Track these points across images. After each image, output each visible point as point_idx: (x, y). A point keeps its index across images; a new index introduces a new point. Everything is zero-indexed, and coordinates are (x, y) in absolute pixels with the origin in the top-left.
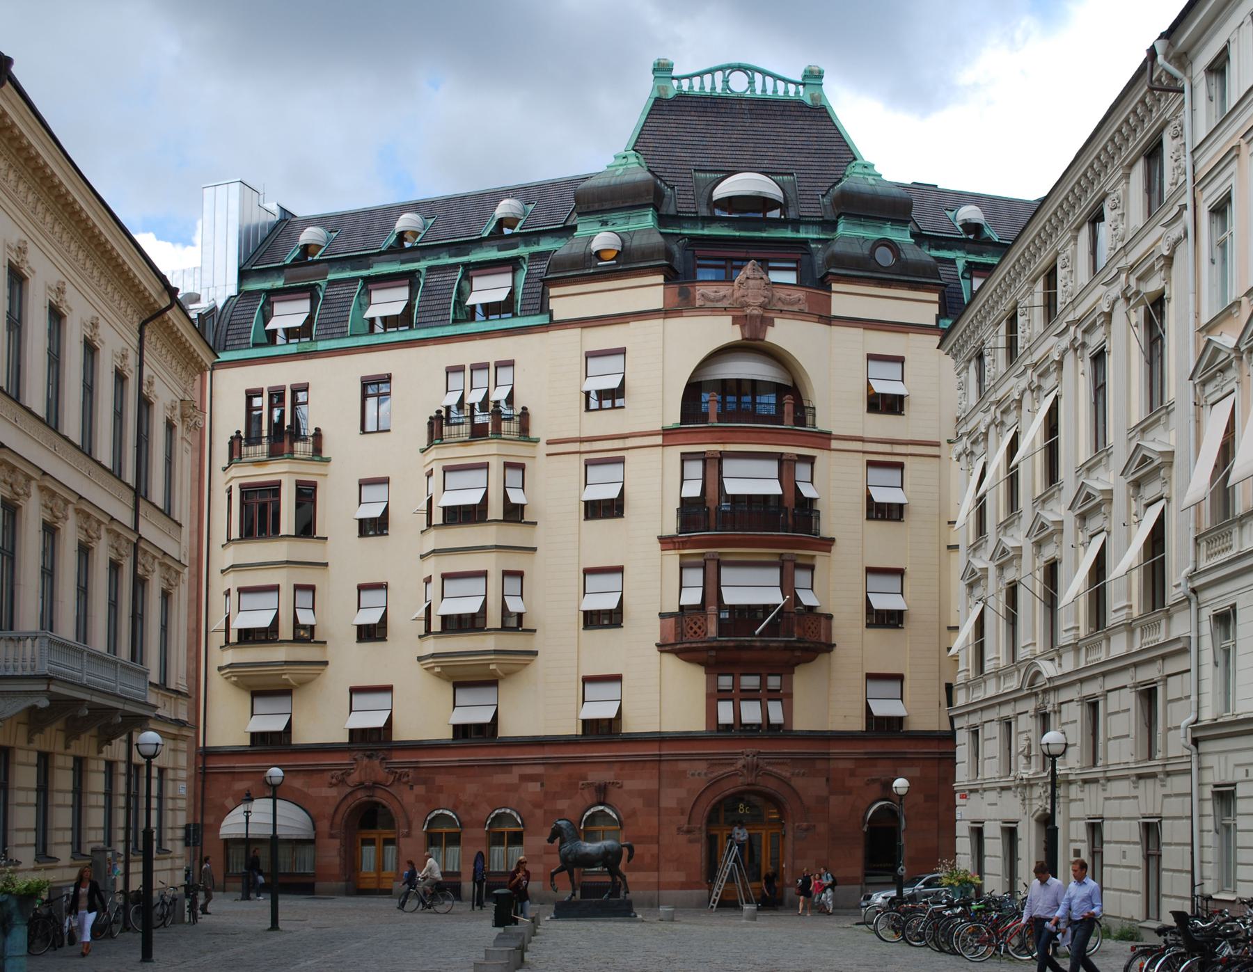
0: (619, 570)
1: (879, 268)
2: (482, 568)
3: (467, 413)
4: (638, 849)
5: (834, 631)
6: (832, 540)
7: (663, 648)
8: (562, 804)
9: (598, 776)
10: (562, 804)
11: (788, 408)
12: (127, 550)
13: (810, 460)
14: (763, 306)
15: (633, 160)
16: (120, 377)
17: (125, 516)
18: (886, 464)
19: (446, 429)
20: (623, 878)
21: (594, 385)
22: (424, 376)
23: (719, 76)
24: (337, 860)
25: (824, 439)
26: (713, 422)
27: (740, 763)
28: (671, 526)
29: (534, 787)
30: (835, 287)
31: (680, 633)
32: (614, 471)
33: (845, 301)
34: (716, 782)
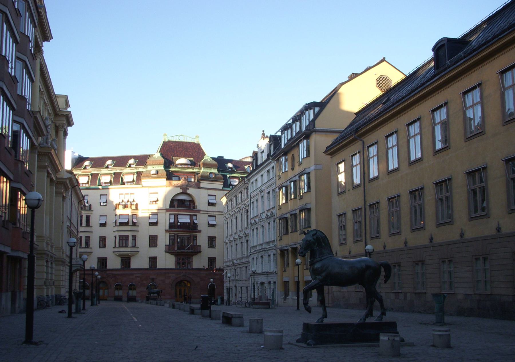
6: (201, 231)
7: (166, 251)
9: (151, 277)
11: (191, 205)
13: (196, 215)
18: (212, 216)
25: (199, 211)
28: (168, 228)
29: (138, 279)
31: (169, 249)
33: (203, 184)
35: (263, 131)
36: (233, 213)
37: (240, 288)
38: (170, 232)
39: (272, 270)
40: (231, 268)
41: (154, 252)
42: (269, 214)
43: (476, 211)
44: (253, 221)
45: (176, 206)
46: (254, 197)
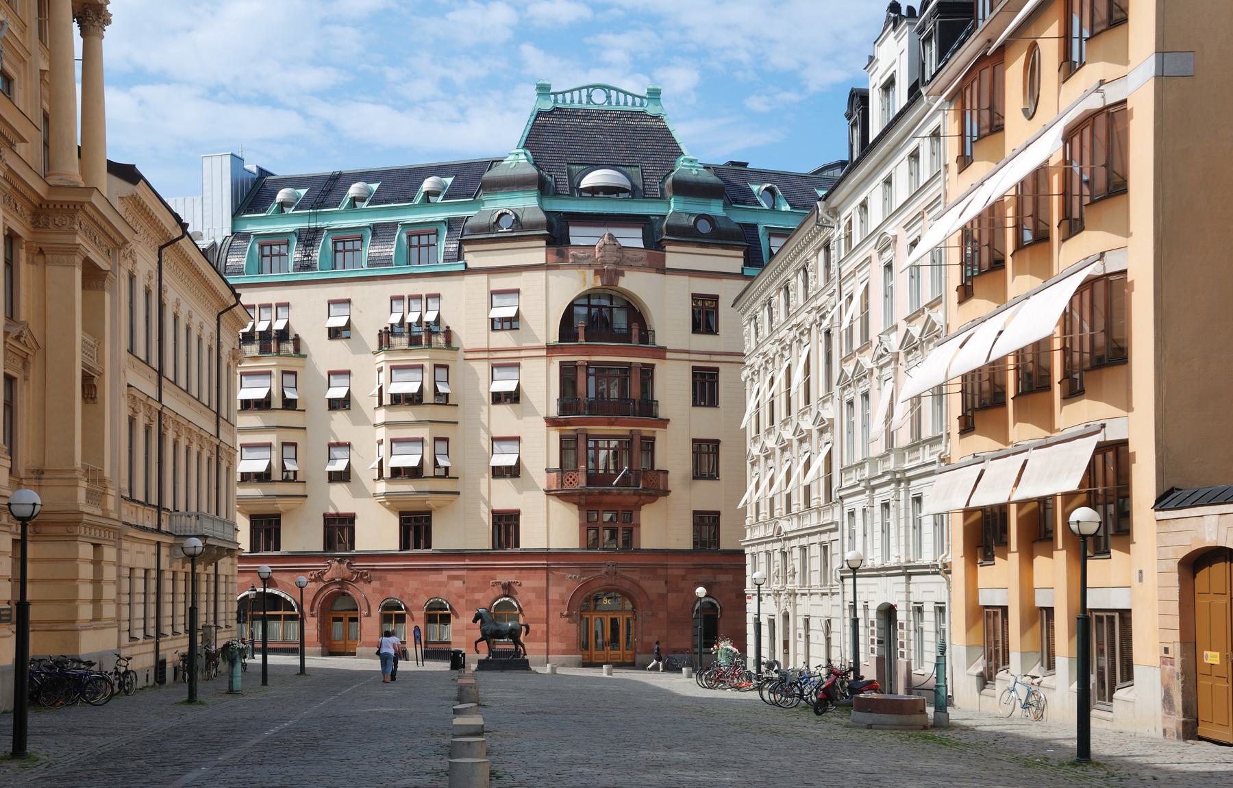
0: (518, 439)
2: (420, 436)
3: (406, 330)
4: (532, 627)
5: (669, 482)
6: (668, 420)
8: (478, 596)
9: (505, 578)
10: (478, 596)
11: (635, 332)
12: (156, 417)
14: (616, 263)
15: (522, 156)
16: (148, 293)
17: (152, 391)
19: (392, 339)
20: (523, 646)
21: (498, 313)
22: (373, 306)
23: (584, 92)
24: (316, 632)
25: (661, 352)
26: (582, 340)
27: (603, 571)
30: (668, 248)
32: (513, 373)
33: (675, 257)
34: (587, 583)
36: (777, 347)
37: (800, 623)
39: (927, 558)
40: (769, 547)
41: (504, 496)
42: (916, 329)
44: (849, 368)
45: (581, 333)
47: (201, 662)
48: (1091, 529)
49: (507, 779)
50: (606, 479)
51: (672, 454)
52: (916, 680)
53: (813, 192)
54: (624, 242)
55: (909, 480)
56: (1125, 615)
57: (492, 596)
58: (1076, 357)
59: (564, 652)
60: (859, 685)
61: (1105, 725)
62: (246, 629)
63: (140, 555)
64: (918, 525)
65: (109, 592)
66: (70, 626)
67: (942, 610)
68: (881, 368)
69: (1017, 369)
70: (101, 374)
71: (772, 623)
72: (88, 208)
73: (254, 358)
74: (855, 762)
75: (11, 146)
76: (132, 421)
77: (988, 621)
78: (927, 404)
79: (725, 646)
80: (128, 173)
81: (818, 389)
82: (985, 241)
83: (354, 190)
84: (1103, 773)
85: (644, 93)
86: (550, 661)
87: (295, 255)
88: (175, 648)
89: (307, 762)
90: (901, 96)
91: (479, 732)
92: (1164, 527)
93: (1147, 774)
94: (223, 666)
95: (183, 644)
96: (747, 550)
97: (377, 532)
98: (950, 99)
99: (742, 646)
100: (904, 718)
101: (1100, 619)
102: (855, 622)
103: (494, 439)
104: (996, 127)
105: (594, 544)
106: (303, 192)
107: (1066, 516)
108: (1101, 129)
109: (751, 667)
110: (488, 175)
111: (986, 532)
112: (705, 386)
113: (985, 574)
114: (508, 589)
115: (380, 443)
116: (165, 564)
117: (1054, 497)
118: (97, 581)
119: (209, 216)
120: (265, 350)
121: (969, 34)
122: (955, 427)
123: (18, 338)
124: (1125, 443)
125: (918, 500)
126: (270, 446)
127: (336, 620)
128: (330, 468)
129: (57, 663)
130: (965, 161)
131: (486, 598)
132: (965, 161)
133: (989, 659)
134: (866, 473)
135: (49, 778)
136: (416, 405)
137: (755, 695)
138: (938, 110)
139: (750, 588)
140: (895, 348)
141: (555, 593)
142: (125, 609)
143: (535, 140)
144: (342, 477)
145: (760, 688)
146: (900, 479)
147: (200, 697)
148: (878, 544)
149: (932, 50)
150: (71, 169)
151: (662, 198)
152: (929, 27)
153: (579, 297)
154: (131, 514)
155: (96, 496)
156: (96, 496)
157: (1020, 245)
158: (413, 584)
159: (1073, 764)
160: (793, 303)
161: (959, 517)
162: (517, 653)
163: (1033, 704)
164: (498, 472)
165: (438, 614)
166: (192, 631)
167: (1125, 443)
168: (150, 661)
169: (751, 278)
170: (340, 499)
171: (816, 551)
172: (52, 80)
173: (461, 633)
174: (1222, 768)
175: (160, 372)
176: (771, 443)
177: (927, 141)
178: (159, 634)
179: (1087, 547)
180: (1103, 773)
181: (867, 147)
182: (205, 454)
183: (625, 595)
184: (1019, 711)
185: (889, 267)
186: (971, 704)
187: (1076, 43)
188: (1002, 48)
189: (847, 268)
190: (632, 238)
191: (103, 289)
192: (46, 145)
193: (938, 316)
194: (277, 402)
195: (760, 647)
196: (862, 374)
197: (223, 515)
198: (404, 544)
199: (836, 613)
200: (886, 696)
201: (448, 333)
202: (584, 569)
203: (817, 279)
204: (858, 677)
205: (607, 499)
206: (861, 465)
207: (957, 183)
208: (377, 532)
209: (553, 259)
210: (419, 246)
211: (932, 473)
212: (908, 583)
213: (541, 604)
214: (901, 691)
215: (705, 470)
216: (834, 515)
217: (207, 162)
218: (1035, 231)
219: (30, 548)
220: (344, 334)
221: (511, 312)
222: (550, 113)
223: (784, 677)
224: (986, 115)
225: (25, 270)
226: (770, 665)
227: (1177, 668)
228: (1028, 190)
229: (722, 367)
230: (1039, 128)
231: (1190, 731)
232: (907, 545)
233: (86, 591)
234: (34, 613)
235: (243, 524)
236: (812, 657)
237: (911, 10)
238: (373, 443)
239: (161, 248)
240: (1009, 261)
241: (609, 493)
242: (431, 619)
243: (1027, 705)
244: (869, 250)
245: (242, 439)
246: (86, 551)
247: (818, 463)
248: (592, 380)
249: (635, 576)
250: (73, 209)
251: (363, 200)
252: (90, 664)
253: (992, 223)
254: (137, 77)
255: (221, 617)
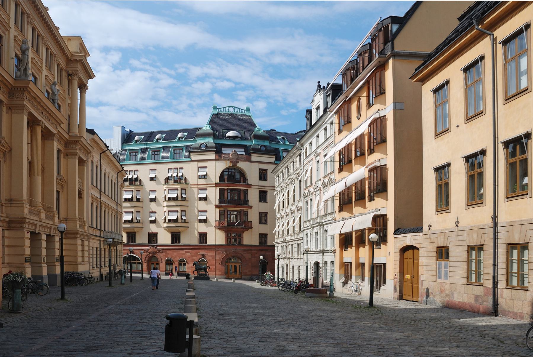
0: (206, 211)
1: (262, 151)
8: (194, 258)
10: (194, 258)
11: (242, 179)
16: (97, 167)
22: (163, 171)
25: (250, 186)
26: (226, 182)
29: (189, 254)
33: (254, 158)
34: (227, 254)
35: (319, 82)
36: (285, 185)
37: (291, 267)
38: (221, 207)
39: (329, 248)
40: (282, 245)
41: (202, 228)
42: (326, 180)
43: (514, 191)
44: (306, 192)
45: (226, 180)
46: (307, 163)
47: (113, 275)
48: (376, 240)
49: (202, 311)
50: (233, 223)
51: (253, 216)
52: (325, 284)
53: (296, 139)
54: (239, 153)
55: (324, 225)
56: (385, 265)
57: (199, 258)
58: (372, 188)
59: (221, 275)
60: (308, 285)
61: (378, 296)
62: (126, 265)
63: (95, 244)
64: (326, 239)
65: (86, 254)
66: (75, 263)
67: (333, 263)
68: (316, 192)
69: (355, 193)
70: (83, 191)
71: (283, 267)
72: (80, 142)
73: (128, 186)
74: (305, 307)
75: (59, 125)
76: (92, 204)
77: (346, 267)
78: (329, 202)
79: (269, 273)
80: (91, 132)
81: (297, 197)
82: (346, 155)
83: (158, 136)
84: (376, 310)
85: (245, 109)
86: (216, 277)
87: (140, 156)
88: (105, 271)
89: (143, 304)
90: (321, 112)
91: (194, 297)
92: (396, 239)
93: (388, 310)
94: (119, 276)
95: (107, 270)
96: (276, 245)
97: (164, 238)
98: (336, 113)
99: (273, 272)
100: (321, 295)
101: (377, 266)
102: (307, 267)
103: (199, 211)
104: (349, 121)
105: (230, 243)
106: (143, 137)
107: (369, 236)
108: (379, 124)
109: (276, 280)
110: (198, 132)
111: (346, 241)
112: (263, 196)
113: (345, 253)
114: (203, 256)
115: (165, 212)
116: (102, 246)
117: (365, 229)
118: (83, 251)
119: (115, 144)
120: (131, 184)
121: (341, 94)
122: (337, 210)
123: (60, 180)
124: (386, 215)
125: (326, 231)
126: (132, 212)
127: (152, 264)
128: (150, 219)
129: (72, 274)
130: (340, 131)
131: (196, 258)
132: (340, 131)
133: (346, 278)
134: (311, 223)
135: (71, 306)
136: (175, 202)
137: (277, 288)
138: (332, 116)
139: (276, 257)
140: (320, 186)
141: (218, 257)
142: (91, 259)
143: (212, 122)
144: (154, 222)
145: (278, 286)
146: (321, 225)
147: (112, 285)
148: (314, 244)
149: (330, 98)
150: (76, 131)
151: (251, 140)
152: (329, 92)
153: (225, 169)
154: (92, 231)
155: (82, 226)
156: (82, 226)
157: (356, 156)
158: (175, 254)
159: (368, 307)
160: (290, 172)
161: (339, 236)
162: (206, 275)
163: (358, 291)
164: (201, 221)
165: (182, 263)
166: (110, 266)
167: (386, 215)
168: (98, 274)
169: (277, 164)
170: (153, 228)
171: (296, 246)
172: (71, 106)
173: (189, 269)
174: (408, 307)
175: (100, 190)
176: (283, 213)
177: (329, 125)
178: (101, 266)
179: (374, 245)
180: (376, 310)
181: (311, 126)
182: (113, 214)
183: (239, 258)
184: (354, 293)
185: (318, 162)
186: (341, 291)
187: (371, 98)
188: (350, 99)
189: (306, 162)
190: (241, 152)
191: (84, 165)
192: (69, 124)
193: (332, 176)
194: (134, 199)
195: (279, 274)
196: (310, 194)
197: (119, 232)
198: (172, 242)
199: (302, 264)
200: (316, 288)
201: (185, 179)
202: (227, 250)
203: (297, 165)
204: (307, 283)
205: (233, 230)
206: (310, 221)
207: (338, 137)
208: (164, 238)
209: (217, 157)
210: (177, 153)
211: (330, 223)
212: (323, 255)
213: (213, 260)
214: (320, 287)
215: (263, 221)
216: (302, 235)
217: (114, 129)
218: (361, 152)
219: (64, 241)
220: (154, 179)
221: (205, 173)
222: (217, 114)
223: (286, 282)
224: (378, 88)
225: (62, 160)
226: (282, 279)
227: (398, 280)
228: (359, 140)
229: (268, 190)
230: (361, 123)
231: (401, 298)
232: (323, 244)
233: (80, 254)
234: (65, 259)
235: (125, 235)
236: (294, 277)
237: (324, 87)
238: (163, 212)
239: (101, 154)
240: (353, 161)
241: (234, 228)
242: (180, 264)
243: (356, 291)
244: (312, 156)
245: (124, 210)
246: (79, 242)
247: (297, 220)
248: (229, 194)
249: (242, 253)
250: (76, 142)
251: (160, 139)
252: (81, 274)
253: (348, 149)
254: (98, 104)
255: (118, 262)
